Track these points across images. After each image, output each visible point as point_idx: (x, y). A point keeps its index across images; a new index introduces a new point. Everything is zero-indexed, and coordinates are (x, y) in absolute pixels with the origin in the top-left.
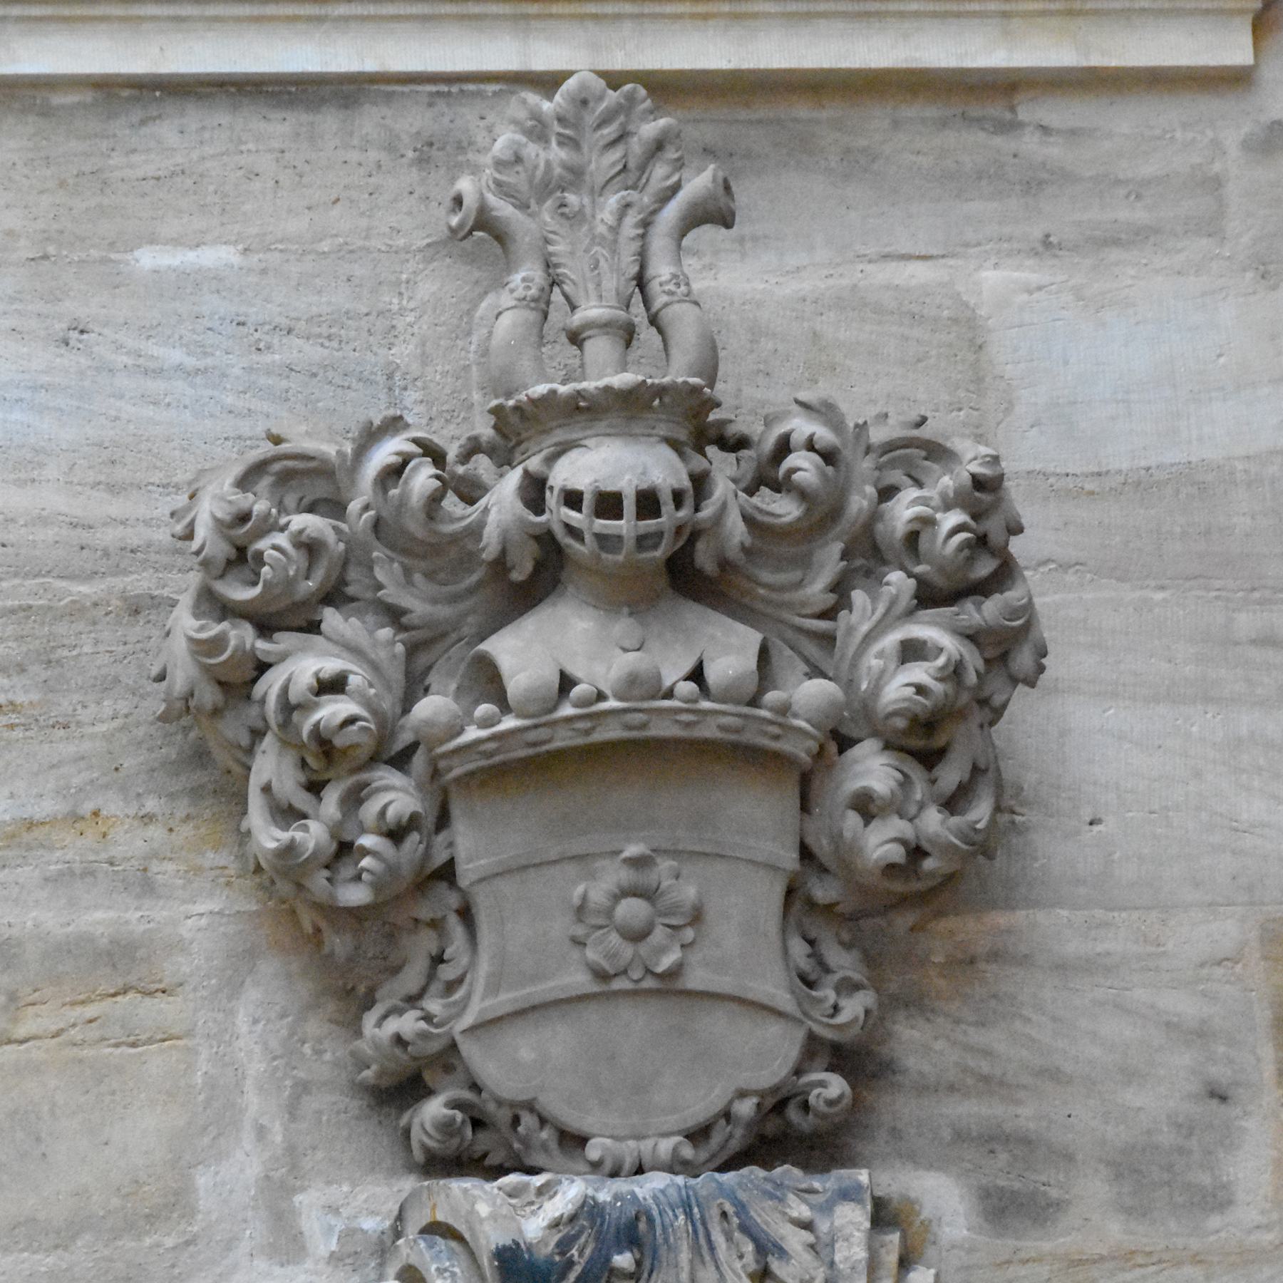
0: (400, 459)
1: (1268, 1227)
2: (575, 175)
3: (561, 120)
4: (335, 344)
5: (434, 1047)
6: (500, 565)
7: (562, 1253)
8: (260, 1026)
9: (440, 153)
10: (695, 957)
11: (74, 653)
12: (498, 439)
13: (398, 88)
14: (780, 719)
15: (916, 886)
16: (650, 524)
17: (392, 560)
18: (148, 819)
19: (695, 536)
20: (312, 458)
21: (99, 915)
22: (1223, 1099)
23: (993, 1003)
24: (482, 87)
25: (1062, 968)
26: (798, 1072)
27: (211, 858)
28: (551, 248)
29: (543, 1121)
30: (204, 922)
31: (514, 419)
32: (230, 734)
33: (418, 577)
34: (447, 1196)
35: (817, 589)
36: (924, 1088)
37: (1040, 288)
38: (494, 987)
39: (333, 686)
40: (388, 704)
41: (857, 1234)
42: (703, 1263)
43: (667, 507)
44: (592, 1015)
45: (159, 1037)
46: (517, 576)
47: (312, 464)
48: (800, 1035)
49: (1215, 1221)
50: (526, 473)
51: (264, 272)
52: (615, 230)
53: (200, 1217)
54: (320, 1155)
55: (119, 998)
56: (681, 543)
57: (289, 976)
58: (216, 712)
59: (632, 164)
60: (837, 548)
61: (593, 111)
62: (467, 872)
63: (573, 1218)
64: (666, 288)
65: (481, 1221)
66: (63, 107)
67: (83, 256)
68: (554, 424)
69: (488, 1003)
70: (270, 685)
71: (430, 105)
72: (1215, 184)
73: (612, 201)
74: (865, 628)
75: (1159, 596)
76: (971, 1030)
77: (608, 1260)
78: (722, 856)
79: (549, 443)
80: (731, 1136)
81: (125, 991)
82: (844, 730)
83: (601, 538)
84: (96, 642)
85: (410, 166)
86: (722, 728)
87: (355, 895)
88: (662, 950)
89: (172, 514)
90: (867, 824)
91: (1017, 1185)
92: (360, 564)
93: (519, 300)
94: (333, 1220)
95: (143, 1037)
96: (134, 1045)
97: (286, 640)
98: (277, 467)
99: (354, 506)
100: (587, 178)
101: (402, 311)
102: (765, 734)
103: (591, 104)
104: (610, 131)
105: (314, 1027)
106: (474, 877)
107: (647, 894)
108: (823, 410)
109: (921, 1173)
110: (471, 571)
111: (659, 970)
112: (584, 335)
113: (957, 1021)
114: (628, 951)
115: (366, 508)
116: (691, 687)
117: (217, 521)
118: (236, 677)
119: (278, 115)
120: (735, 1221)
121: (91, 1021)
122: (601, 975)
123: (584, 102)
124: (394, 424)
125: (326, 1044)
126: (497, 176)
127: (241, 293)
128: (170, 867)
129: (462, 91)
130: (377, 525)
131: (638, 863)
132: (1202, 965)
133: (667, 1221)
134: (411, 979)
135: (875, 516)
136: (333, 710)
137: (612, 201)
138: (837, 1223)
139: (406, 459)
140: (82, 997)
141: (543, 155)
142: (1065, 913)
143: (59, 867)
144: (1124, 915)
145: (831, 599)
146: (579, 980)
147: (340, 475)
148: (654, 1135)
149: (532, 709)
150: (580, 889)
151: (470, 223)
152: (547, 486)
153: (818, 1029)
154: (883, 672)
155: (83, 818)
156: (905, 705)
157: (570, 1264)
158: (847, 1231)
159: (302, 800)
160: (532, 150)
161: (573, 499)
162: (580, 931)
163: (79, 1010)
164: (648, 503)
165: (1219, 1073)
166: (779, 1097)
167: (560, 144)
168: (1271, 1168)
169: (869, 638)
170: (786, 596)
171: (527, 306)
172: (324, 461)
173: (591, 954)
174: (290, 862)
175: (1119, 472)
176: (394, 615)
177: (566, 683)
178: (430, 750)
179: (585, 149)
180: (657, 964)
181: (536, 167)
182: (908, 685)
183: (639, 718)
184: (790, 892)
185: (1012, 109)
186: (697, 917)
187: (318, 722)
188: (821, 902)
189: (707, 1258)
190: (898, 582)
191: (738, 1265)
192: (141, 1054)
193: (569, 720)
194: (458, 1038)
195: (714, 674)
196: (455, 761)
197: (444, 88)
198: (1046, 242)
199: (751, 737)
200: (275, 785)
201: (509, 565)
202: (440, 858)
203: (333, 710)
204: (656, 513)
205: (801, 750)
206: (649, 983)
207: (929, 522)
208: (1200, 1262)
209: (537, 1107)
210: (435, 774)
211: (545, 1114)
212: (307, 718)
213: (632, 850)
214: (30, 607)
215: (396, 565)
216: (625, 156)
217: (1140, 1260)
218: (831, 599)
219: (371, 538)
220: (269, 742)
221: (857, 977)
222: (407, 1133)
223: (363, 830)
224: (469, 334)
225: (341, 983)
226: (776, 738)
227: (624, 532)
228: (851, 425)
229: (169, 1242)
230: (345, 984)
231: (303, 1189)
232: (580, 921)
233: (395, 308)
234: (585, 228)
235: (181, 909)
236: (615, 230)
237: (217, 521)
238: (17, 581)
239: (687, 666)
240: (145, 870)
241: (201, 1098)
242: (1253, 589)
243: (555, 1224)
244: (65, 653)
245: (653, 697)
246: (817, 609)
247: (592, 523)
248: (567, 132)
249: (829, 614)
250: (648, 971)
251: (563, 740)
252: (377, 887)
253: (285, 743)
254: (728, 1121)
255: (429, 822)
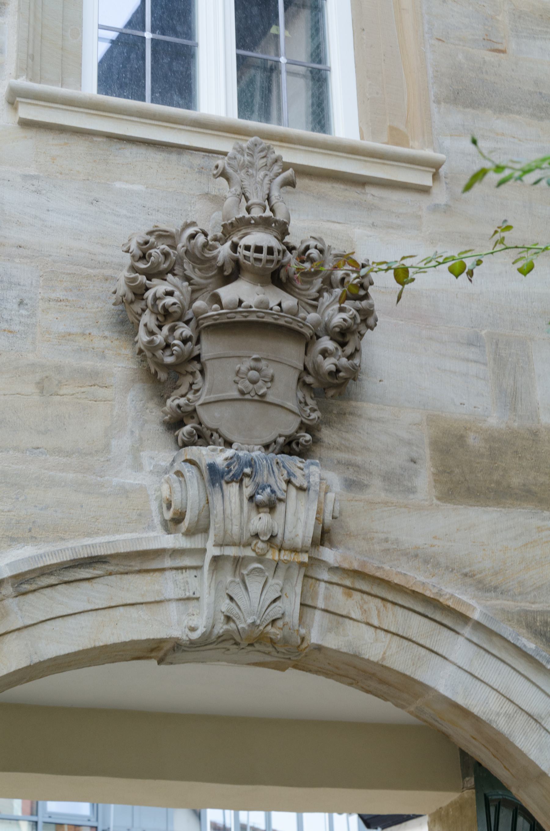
0: (195, 233)
1: (426, 500)
2: (251, 165)
3: (248, 148)
4: (171, 216)
5: (190, 409)
6: (221, 269)
7: (228, 467)
8: (134, 402)
9: (205, 171)
10: (270, 392)
11: (87, 288)
12: (223, 236)
13: (194, 152)
14: (303, 322)
15: (336, 381)
16: (270, 257)
17: (190, 263)
18: (106, 337)
19: (282, 266)
20: (167, 232)
21: (89, 363)
22: (415, 462)
23: (350, 427)
24: (218, 156)
25: (370, 419)
26: (297, 432)
27: (124, 351)
28: (243, 183)
29: (220, 436)
30: (120, 369)
31: (229, 228)
32: (135, 310)
33: (196, 270)
34: (192, 450)
35: (313, 291)
36: (329, 448)
37: (371, 236)
38: (210, 392)
39: (170, 294)
40: (186, 304)
41: (316, 474)
42: (271, 476)
43: (276, 253)
44: (238, 405)
45: (104, 400)
46: (226, 273)
47: (168, 234)
48: (298, 420)
49: (411, 496)
50: (233, 242)
51: (151, 194)
52: (263, 180)
53: (112, 453)
54: (149, 442)
55: (93, 387)
56: (278, 266)
57: (144, 389)
58: (132, 302)
59: (268, 164)
60: (320, 280)
61: (258, 147)
62: (204, 357)
63: (232, 458)
64: (277, 198)
65: (203, 455)
66: (96, 141)
67: (99, 181)
68: (243, 228)
69: (207, 397)
70: (149, 294)
71: (203, 158)
72: (419, 217)
73: (262, 173)
74: (327, 303)
75: (401, 322)
76: (344, 433)
77: (242, 470)
78: (281, 363)
79: (240, 234)
80: (275, 449)
81: (94, 385)
82: (318, 334)
83: (256, 259)
84: (94, 286)
85: (196, 173)
86: (286, 322)
87: (169, 360)
88: (261, 388)
89: (123, 245)
90: (324, 359)
91: (355, 479)
92: (179, 264)
93: (234, 194)
94: (152, 461)
95: (99, 399)
96: (96, 401)
97: (155, 281)
98: (157, 233)
99: (180, 246)
100: (255, 166)
101: (191, 211)
102: (298, 326)
103: (258, 146)
104: (263, 154)
105: (151, 405)
106: (207, 358)
107: (258, 370)
108: (319, 240)
109: (327, 471)
110: (212, 271)
111: (260, 394)
112: (252, 207)
113: (340, 430)
114: (251, 386)
115: (183, 246)
116: (278, 308)
117: (139, 244)
118: (139, 292)
119: (159, 153)
120: (281, 465)
121: (83, 392)
122: (242, 393)
123: (256, 145)
124: (193, 224)
125: (154, 410)
126: (229, 161)
127: (144, 198)
128: (111, 352)
129: (212, 156)
130: (186, 252)
131: (257, 360)
132: (410, 424)
133: (260, 463)
134: (183, 389)
135: (331, 273)
136: (169, 300)
137: (262, 173)
138: (311, 471)
139: (197, 233)
140: (81, 385)
141: (242, 158)
142: (371, 404)
143: (77, 347)
144: (389, 407)
145: (317, 295)
146: (235, 394)
147: (177, 238)
148: (253, 444)
149: (231, 307)
150: (239, 366)
151: (219, 174)
152: (239, 245)
153: (304, 420)
154: (333, 315)
155: (86, 334)
156: (340, 324)
157: (230, 471)
158: (314, 473)
159: (156, 330)
160: (239, 156)
161: (247, 248)
162: (237, 379)
163: (80, 389)
164: (270, 251)
165: (414, 455)
166: (291, 439)
167: (248, 155)
168: (428, 484)
169: (328, 307)
170: (304, 293)
171: (236, 197)
172: (172, 233)
173: (240, 386)
174: (152, 345)
175: (391, 288)
176: (188, 279)
177: (240, 302)
178: (197, 318)
179: (255, 158)
180: (259, 392)
181: (240, 161)
182: (341, 318)
183: (261, 314)
184: (299, 379)
185: (365, 191)
186: (272, 380)
187: (165, 303)
188: (307, 383)
189: (272, 474)
190: (338, 291)
191: (281, 478)
192: (98, 404)
193: (241, 312)
194: (197, 407)
195: (283, 305)
196: (205, 321)
197: (207, 154)
198: (373, 224)
199: (294, 326)
200: (148, 324)
201: (224, 269)
202: (196, 353)
203: (169, 300)
204: (272, 254)
205: (308, 332)
206: (256, 398)
207: (348, 275)
208: (406, 507)
209: (219, 431)
210: (198, 326)
211: (221, 434)
212: (161, 302)
213: (255, 356)
214: (75, 274)
215: (190, 265)
216: (267, 162)
217: (390, 505)
218: (317, 295)
219: (184, 255)
220: (147, 311)
221: (316, 407)
222: (177, 436)
223: (174, 339)
224: (209, 221)
225: (159, 393)
226: (301, 327)
227: (263, 258)
228: (327, 246)
229: (102, 459)
230: (161, 394)
231: (143, 451)
232: (237, 375)
233: (189, 209)
234: (254, 178)
235: (114, 364)
236: (263, 180)
237: (139, 244)
238: (71, 266)
239: (277, 302)
240: (103, 352)
241: (115, 419)
242: (427, 325)
243: (226, 459)
244: (85, 288)
245: (266, 309)
246: (312, 297)
247: (253, 254)
248: (251, 152)
249: (316, 299)
250: (256, 394)
251: (239, 318)
252: (178, 357)
253: (152, 312)
254: (275, 444)
255: (194, 339)
